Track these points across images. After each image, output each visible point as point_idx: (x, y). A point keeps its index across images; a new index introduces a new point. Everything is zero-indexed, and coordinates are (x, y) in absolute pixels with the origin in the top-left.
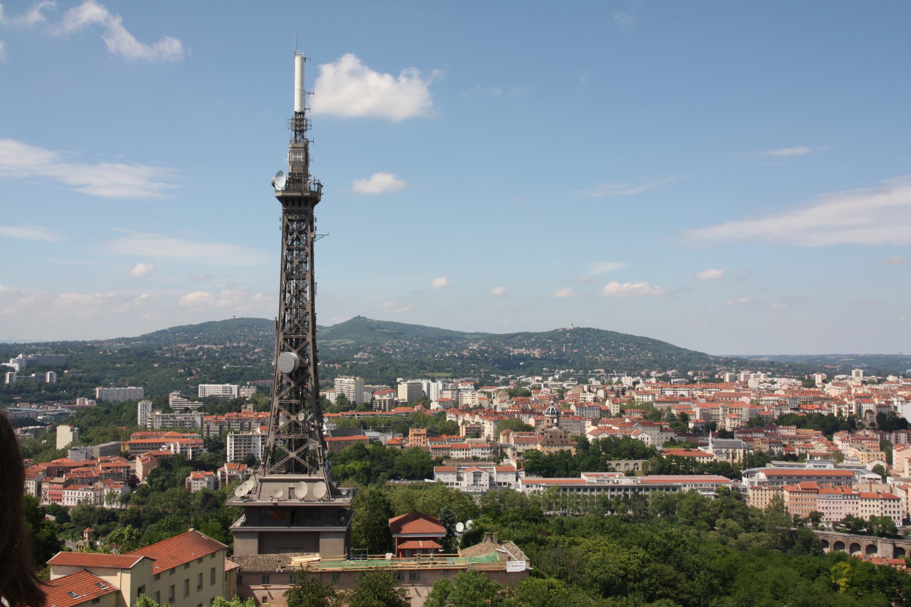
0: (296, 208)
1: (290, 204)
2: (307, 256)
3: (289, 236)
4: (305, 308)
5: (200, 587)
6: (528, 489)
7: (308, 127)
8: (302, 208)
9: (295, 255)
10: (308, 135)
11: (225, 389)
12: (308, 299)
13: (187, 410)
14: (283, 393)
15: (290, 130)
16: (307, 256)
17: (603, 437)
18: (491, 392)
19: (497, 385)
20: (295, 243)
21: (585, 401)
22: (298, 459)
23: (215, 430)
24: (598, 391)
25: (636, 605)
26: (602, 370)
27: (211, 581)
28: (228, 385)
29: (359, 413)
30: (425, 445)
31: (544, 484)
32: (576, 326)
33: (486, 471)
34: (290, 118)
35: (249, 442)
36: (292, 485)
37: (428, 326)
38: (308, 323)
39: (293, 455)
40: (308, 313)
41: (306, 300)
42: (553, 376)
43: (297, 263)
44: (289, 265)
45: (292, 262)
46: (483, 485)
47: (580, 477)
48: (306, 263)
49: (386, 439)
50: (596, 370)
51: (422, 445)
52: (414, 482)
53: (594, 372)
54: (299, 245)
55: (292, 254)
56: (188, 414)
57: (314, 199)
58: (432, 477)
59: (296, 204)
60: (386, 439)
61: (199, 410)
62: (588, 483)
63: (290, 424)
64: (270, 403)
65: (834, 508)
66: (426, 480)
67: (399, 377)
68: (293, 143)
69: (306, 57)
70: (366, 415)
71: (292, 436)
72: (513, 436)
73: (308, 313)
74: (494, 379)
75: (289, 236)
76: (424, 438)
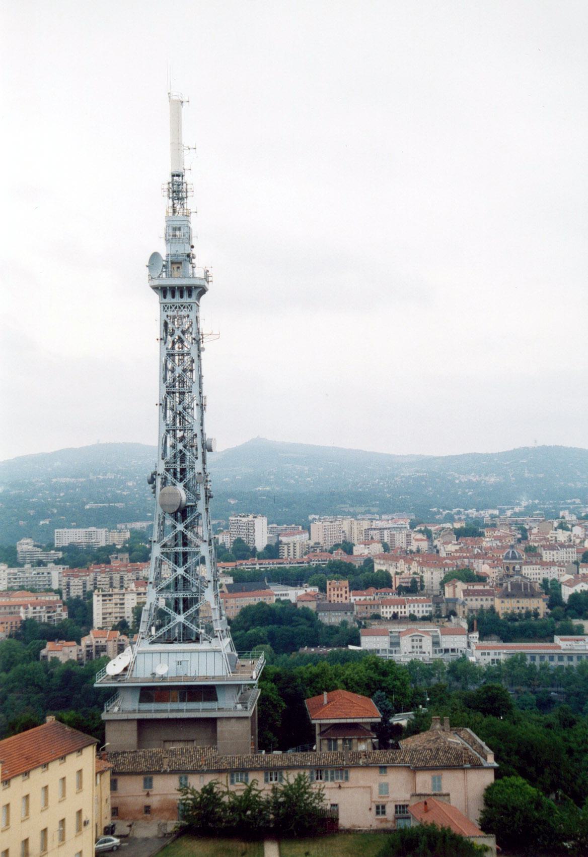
0: (177, 300)
1: (169, 295)
2: (193, 361)
3: (169, 337)
4: (192, 430)
5: (62, 838)
6: (484, 657)
7: (189, 194)
8: (186, 300)
9: (177, 361)
10: (190, 204)
11: (90, 534)
12: (195, 417)
13: (40, 563)
14: (166, 539)
15: (166, 198)
16: (193, 361)
17: (582, 589)
18: (180, 469)
19: (440, 522)
20: (176, 346)
21: (556, 541)
22: (188, 624)
23: (76, 592)
24: (573, 528)
25: (587, 777)
26: (578, 501)
27: (77, 830)
28: (92, 529)
29: (261, 561)
30: (347, 601)
31: (505, 651)
32: (540, 444)
33: (429, 635)
34: (166, 182)
35: (122, 602)
36: (180, 657)
37: (461, 453)
38: (197, 449)
39: (180, 618)
40: (196, 435)
41: (193, 417)
42: (513, 509)
43: (181, 372)
44: (169, 374)
45: (173, 371)
46: (424, 653)
47: (552, 641)
48: (191, 371)
49: (293, 594)
50: (569, 501)
51: (344, 601)
52: (335, 649)
53: (566, 503)
54: (182, 348)
55: (174, 361)
56: (41, 569)
57: (196, 291)
58: (358, 644)
59: (177, 295)
60: (293, 594)
61: (57, 562)
62: (564, 650)
63: (176, 578)
64: (149, 551)
65: (536, 574)
66: (351, 647)
67: (311, 514)
68: (170, 214)
69: (184, 100)
70: (271, 565)
71: (180, 595)
72: (461, 586)
73: (196, 435)
74: (435, 514)
75: (169, 337)
76: (346, 592)
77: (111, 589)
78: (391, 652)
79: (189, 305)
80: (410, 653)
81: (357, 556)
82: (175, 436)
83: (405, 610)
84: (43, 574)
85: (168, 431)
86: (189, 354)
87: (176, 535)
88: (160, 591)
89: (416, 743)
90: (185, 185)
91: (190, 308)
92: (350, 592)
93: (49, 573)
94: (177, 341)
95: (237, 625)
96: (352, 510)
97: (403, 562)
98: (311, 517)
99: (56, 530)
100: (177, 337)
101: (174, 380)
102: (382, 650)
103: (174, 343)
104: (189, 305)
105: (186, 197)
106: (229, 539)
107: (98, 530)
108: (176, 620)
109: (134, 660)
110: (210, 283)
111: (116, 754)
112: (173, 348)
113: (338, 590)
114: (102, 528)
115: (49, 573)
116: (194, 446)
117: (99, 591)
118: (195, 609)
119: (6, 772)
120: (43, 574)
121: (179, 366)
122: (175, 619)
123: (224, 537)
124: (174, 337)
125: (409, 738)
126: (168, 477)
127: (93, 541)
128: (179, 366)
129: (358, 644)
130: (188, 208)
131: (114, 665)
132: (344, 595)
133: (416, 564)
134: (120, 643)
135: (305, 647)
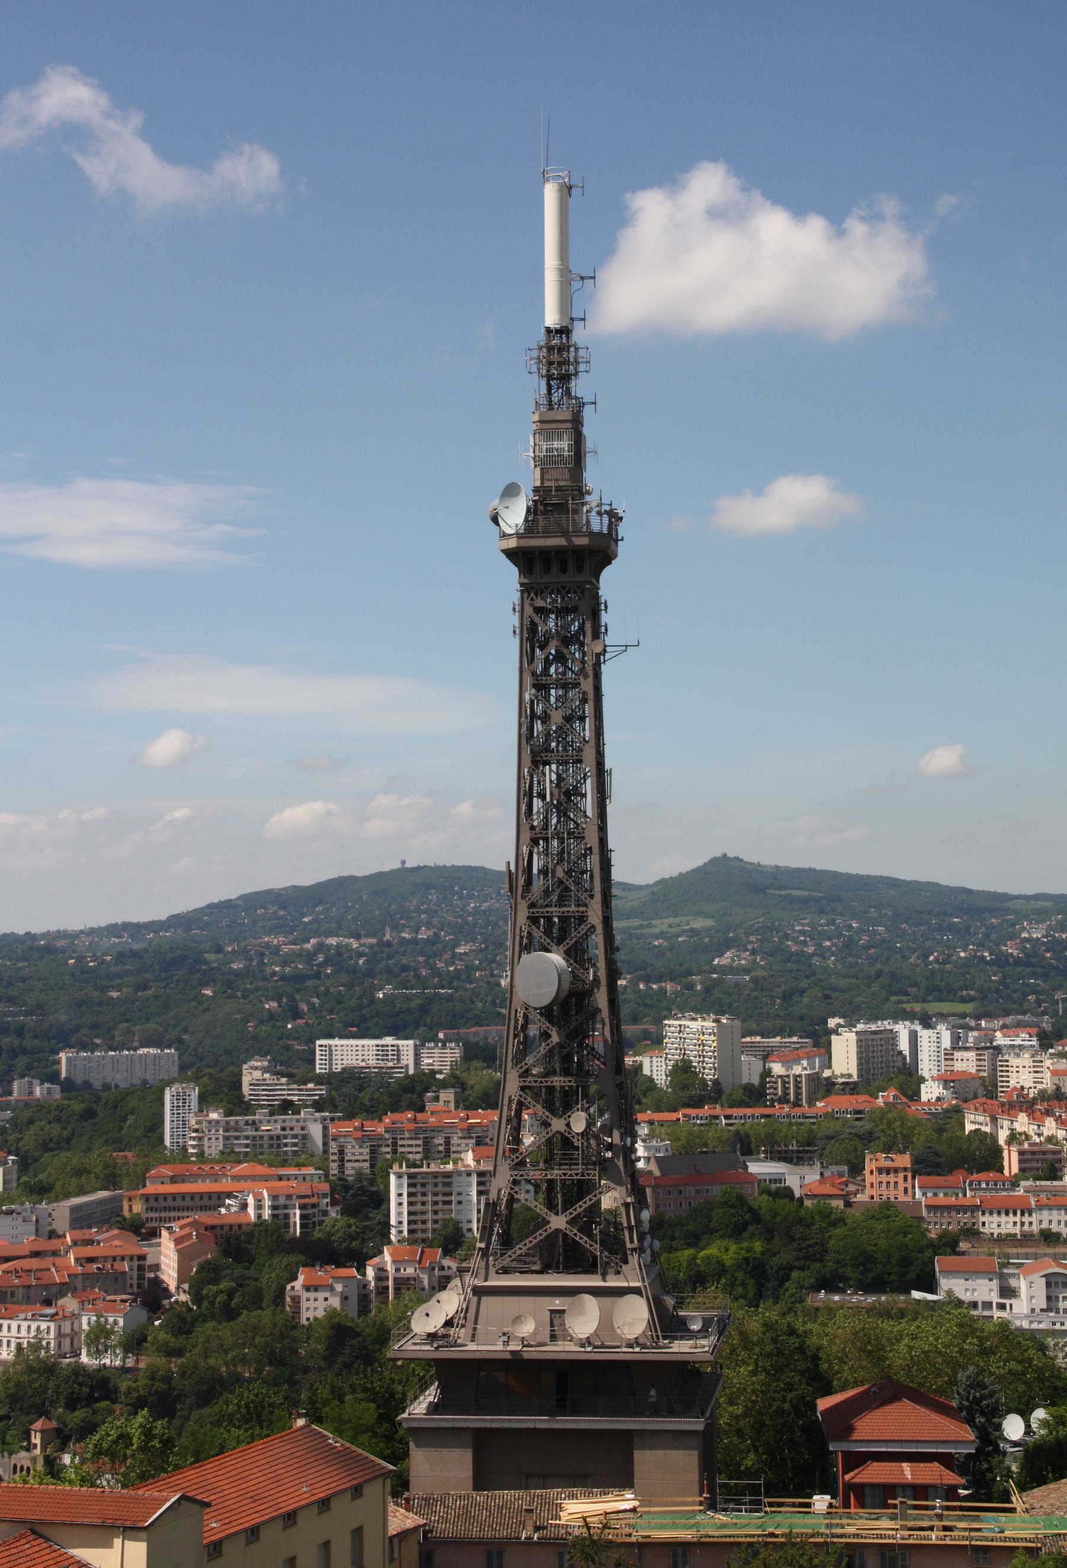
2: (584, 701)
3: (538, 651)
4: (583, 838)
7: (582, 367)
9: (553, 700)
10: (580, 387)
12: (589, 813)
13: (287, 1106)
16: (584, 701)
22: (573, 1233)
28: (389, 1040)
30: (909, 1199)
36: (557, 1303)
38: (592, 877)
39: (558, 1222)
40: (590, 849)
43: (560, 721)
44: (538, 726)
45: (545, 718)
54: (564, 674)
55: (547, 698)
58: (932, 1288)
63: (549, 1141)
66: (916, 1295)
73: (590, 849)
75: (538, 651)
77: (453, 1156)
78: (1002, 1307)
79: (579, 587)
80: (1042, 1310)
81: (925, 1104)
82: (546, 852)
83: (1031, 1219)
84: (292, 1129)
85: (535, 841)
86: (577, 685)
87: (551, 1051)
88: (517, 1164)
89: (1052, 1501)
90: (572, 349)
91: (579, 592)
92: (913, 1178)
93: (303, 1128)
94: (554, 659)
95: (703, 1093)
96: (917, 1007)
97: (1026, 1119)
98: (832, 1023)
99: (318, 1042)
100: (553, 652)
101: (548, 735)
102: (983, 1303)
103: (547, 663)
104: (579, 587)
105: (576, 374)
106: (663, 1064)
107: (400, 1042)
108: (566, 1219)
109: (464, 1306)
110: (620, 543)
111: (428, 1501)
112: (546, 671)
113: (1023, 1214)
114: (407, 1038)
115: (303, 1128)
116: (586, 872)
117: (401, 1167)
118: (589, 1203)
119: (214, 1525)
120: (292, 1129)
121: (556, 709)
122: (549, 1222)
123: (654, 1059)
124: (546, 651)
125: (1035, 1490)
126: (534, 934)
127: (391, 1064)
128: (556, 709)
129: (932, 1288)
130: (579, 396)
131: (427, 1315)
132: (901, 1185)
133: (1054, 1124)
134: (443, 1273)
135: (819, 1291)
